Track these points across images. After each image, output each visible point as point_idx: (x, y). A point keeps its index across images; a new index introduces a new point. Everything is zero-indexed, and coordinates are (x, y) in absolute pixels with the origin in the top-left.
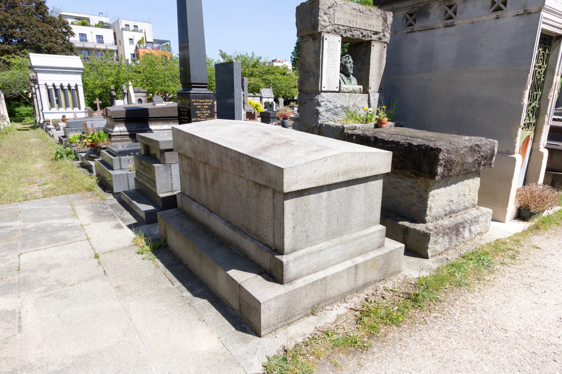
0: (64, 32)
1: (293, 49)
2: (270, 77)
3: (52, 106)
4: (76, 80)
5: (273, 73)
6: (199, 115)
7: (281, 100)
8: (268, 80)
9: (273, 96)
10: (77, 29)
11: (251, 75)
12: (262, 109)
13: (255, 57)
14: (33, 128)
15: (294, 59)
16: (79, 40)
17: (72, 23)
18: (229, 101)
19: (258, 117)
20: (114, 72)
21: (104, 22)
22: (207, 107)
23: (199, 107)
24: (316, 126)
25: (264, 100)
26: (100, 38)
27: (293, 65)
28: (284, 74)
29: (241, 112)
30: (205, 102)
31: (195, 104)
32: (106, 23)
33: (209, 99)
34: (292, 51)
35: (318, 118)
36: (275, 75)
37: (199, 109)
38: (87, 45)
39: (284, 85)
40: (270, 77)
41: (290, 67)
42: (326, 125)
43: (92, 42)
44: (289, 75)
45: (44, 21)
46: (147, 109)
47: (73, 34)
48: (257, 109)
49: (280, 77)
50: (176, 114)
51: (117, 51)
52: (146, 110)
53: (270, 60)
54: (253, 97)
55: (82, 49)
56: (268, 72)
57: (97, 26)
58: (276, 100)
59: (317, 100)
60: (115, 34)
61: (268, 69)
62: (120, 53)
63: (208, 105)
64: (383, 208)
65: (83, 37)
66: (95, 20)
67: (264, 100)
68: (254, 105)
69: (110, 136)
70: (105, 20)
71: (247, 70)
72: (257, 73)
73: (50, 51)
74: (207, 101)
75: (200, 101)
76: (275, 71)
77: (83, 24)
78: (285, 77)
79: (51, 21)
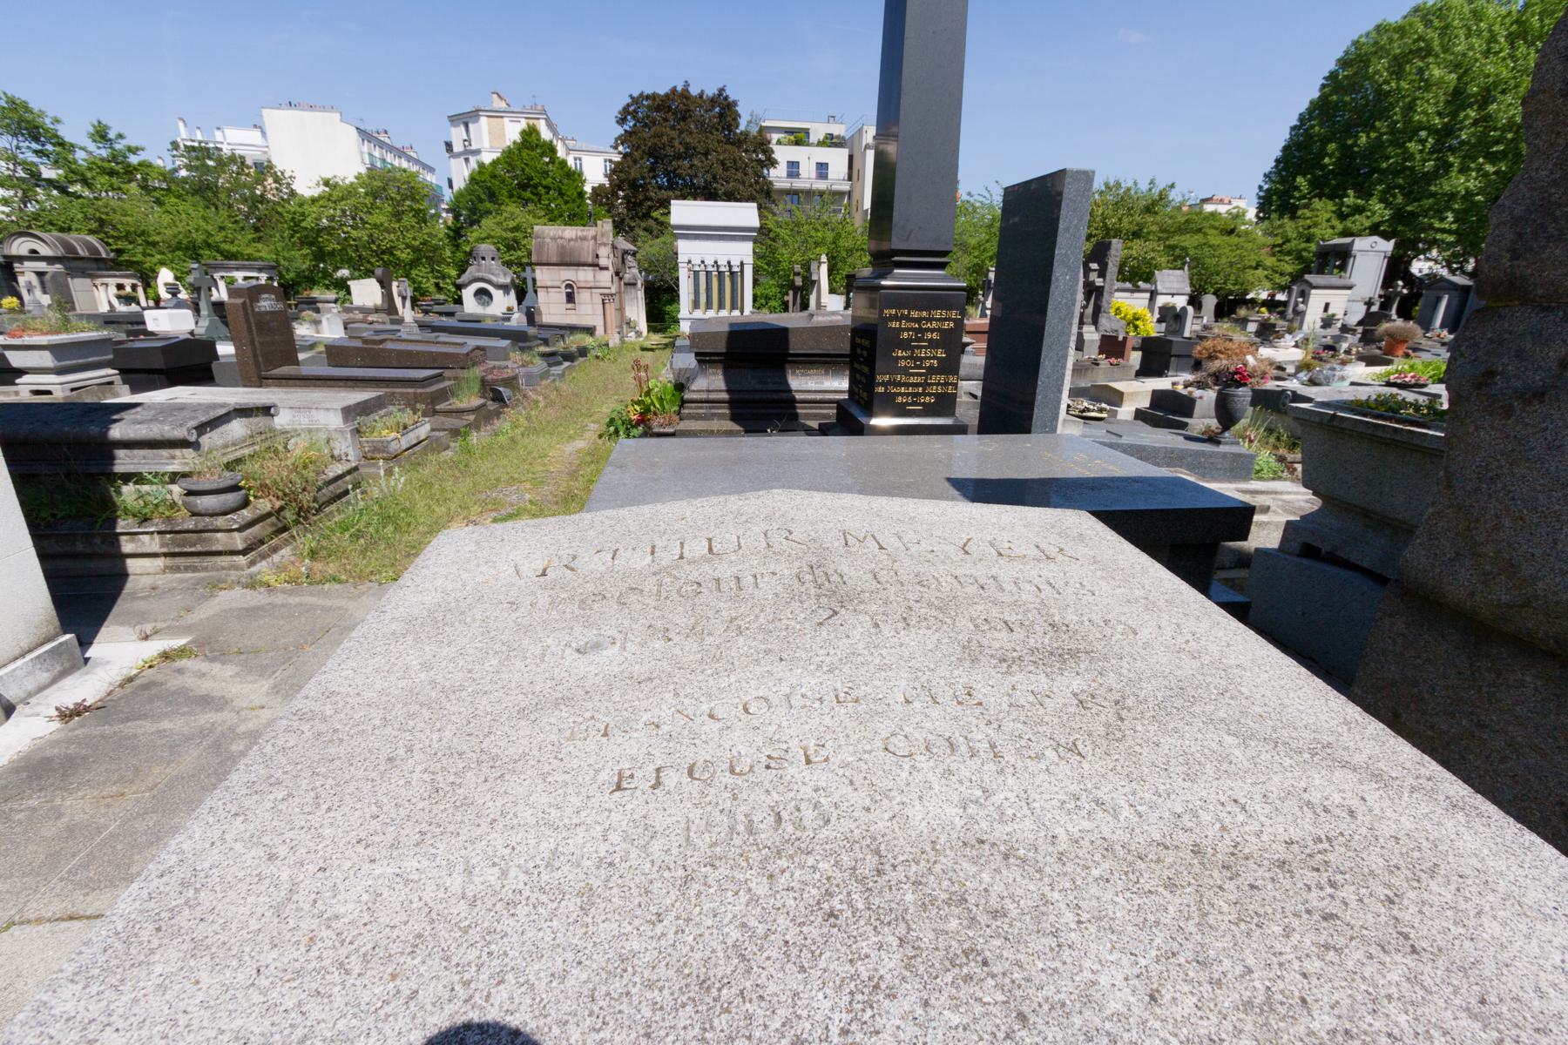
0: (760, 161)
1: (1269, 165)
2: (1189, 241)
4: (742, 253)
5: (1199, 230)
7: (1210, 301)
8: (1183, 249)
9: (1188, 290)
10: (783, 154)
11: (1136, 235)
12: (1152, 327)
13: (1161, 184)
15: (1268, 190)
16: (784, 174)
17: (779, 142)
19: (1134, 349)
20: (830, 236)
21: (836, 133)
22: (935, 336)
25: (1161, 301)
26: (822, 169)
27: (1261, 208)
28: (1232, 232)
29: (1065, 356)
30: (929, 320)
31: (895, 325)
32: (838, 137)
33: (949, 307)
34: (1267, 170)
36: (1205, 234)
37: (905, 345)
38: (798, 184)
39: (1224, 260)
40: (1189, 241)
41: (1251, 214)
43: (808, 178)
44: (1247, 233)
45: (728, 142)
46: (784, 332)
47: (773, 163)
48: (1136, 327)
49: (1215, 239)
50: (845, 348)
51: (850, 193)
52: (783, 333)
53: (1194, 198)
54: (1132, 291)
55: (788, 192)
56: (1187, 227)
57: (821, 144)
58: (1195, 301)
60: (851, 158)
61: (1187, 221)
62: (855, 197)
65: (793, 167)
66: (818, 133)
67: (1161, 301)
68: (1130, 317)
70: (838, 130)
71: (1125, 220)
72: (1155, 228)
73: (711, 195)
74: (937, 314)
75: (915, 314)
76: (1205, 224)
77: (798, 143)
78: (1234, 239)
79: (740, 141)
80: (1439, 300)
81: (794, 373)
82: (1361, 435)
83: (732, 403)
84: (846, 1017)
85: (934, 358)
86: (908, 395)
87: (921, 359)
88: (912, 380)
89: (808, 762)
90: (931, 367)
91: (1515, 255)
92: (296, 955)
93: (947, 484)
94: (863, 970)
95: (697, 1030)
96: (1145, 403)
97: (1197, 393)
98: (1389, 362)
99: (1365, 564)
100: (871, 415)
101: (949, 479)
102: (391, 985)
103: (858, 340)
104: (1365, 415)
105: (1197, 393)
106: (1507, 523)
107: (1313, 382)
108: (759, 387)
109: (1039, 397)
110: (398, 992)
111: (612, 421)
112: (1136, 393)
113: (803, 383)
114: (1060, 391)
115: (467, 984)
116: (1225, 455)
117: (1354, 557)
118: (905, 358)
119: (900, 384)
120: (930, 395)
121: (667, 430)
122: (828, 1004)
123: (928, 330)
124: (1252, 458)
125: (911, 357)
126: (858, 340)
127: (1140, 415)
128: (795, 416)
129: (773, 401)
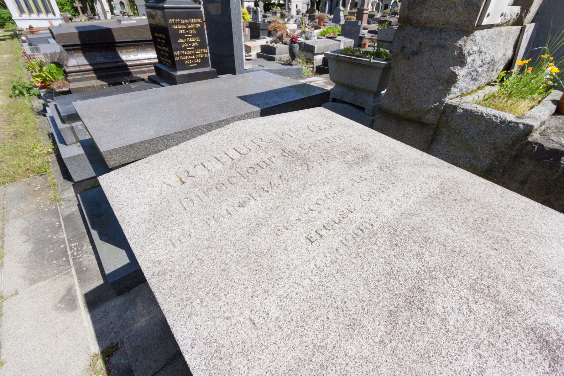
3: (22, 11)
6: (183, 45)
14: (12, 37)
18: (96, 328)
22: (194, 31)
23: (181, 32)
24: (436, 109)
30: (190, 24)
31: (175, 27)
35: (447, 91)
37: (182, 36)
42: (465, 111)
59: (461, 49)
63: (195, 28)
64: (488, 173)
69: (66, 74)
74: (192, 20)
75: (183, 21)
80: (326, 3)
81: (121, 52)
82: (345, 62)
83: (95, 71)
84: (420, 263)
85: (196, 42)
86: (189, 59)
87: (191, 43)
88: (189, 53)
89: (352, 212)
90: (195, 47)
91: (409, 10)
92: (280, 333)
93: (239, 100)
94: (413, 252)
95: (398, 283)
96: (259, 51)
97: (275, 45)
98: (320, 28)
99: (349, 102)
100: (176, 70)
101: (238, 97)
102: (319, 321)
103: (156, 35)
104: (346, 55)
105: (275, 45)
106: (409, 90)
107: (307, 38)
108: (106, 61)
109: (235, 55)
110: (323, 321)
111: (14, 88)
112: (254, 47)
113: (129, 57)
114: (242, 51)
115: (337, 308)
116: (294, 69)
117: (346, 100)
118: (184, 43)
119: (185, 55)
120: (198, 58)
121: (64, 89)
122: (415, 263)
123: (190, 29)
124: (302, 69)
125: (186, 42)
126: (156, 35)
127: (259, 56)
128: (130, 73)
129: (112, 68)
